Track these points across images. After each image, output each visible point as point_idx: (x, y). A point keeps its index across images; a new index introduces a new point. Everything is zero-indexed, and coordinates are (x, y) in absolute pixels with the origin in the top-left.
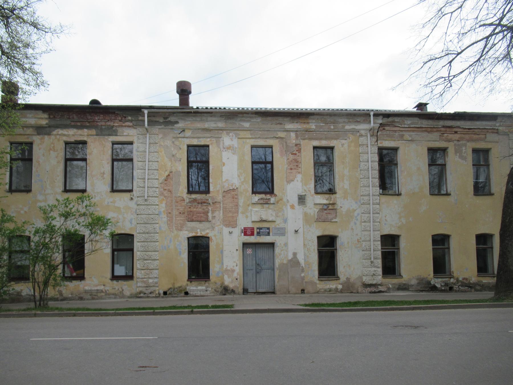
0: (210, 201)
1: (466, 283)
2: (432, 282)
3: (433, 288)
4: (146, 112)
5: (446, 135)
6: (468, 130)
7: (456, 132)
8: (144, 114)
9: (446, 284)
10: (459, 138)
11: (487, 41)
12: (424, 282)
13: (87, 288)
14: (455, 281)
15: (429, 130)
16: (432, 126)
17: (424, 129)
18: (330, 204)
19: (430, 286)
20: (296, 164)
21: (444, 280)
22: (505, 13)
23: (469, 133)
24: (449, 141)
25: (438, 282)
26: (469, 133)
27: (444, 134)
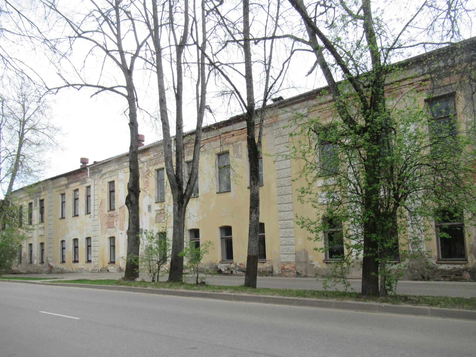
0: (115, 215)
1: (242, 268)
2: (219, 267)
3: (220, 272)
4: (88, 168)
5: (227, 139)
6: (241, 131)
7: (233, 135)
8: (87, 169)
9: (228, 269)
10: (236, 139)
11: (58, 90)
12: (214, 266)
13: (79, 267)
14: (235, 266)
15: (214, 139)
16: (215, 136)
17: (210, 140)
18: (161, 210)
19: (217, 270)
20: (147, 184)
21: (227, 265)
22: (194, 24)
23: (242, 133)
24: (228, 144)
25: (223, 267)
26: (242, 133)
27: (225, 139)
